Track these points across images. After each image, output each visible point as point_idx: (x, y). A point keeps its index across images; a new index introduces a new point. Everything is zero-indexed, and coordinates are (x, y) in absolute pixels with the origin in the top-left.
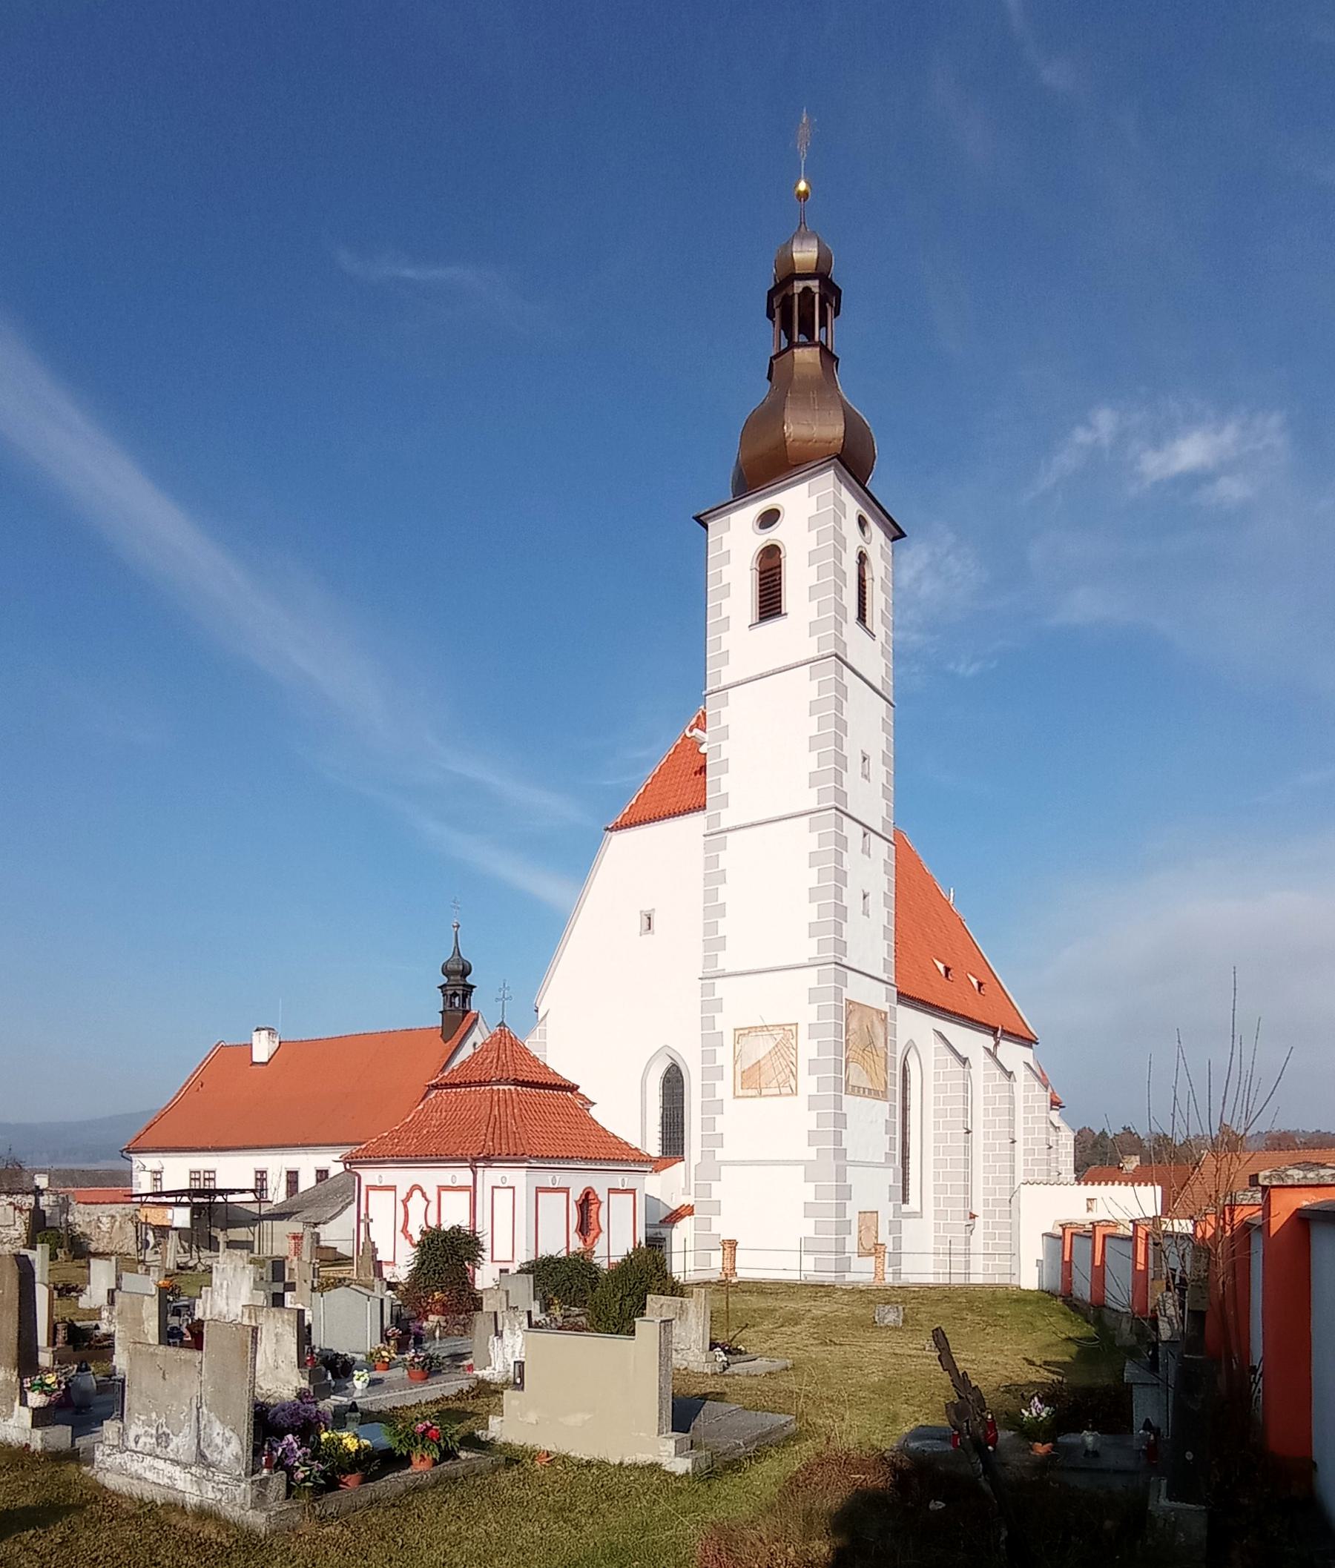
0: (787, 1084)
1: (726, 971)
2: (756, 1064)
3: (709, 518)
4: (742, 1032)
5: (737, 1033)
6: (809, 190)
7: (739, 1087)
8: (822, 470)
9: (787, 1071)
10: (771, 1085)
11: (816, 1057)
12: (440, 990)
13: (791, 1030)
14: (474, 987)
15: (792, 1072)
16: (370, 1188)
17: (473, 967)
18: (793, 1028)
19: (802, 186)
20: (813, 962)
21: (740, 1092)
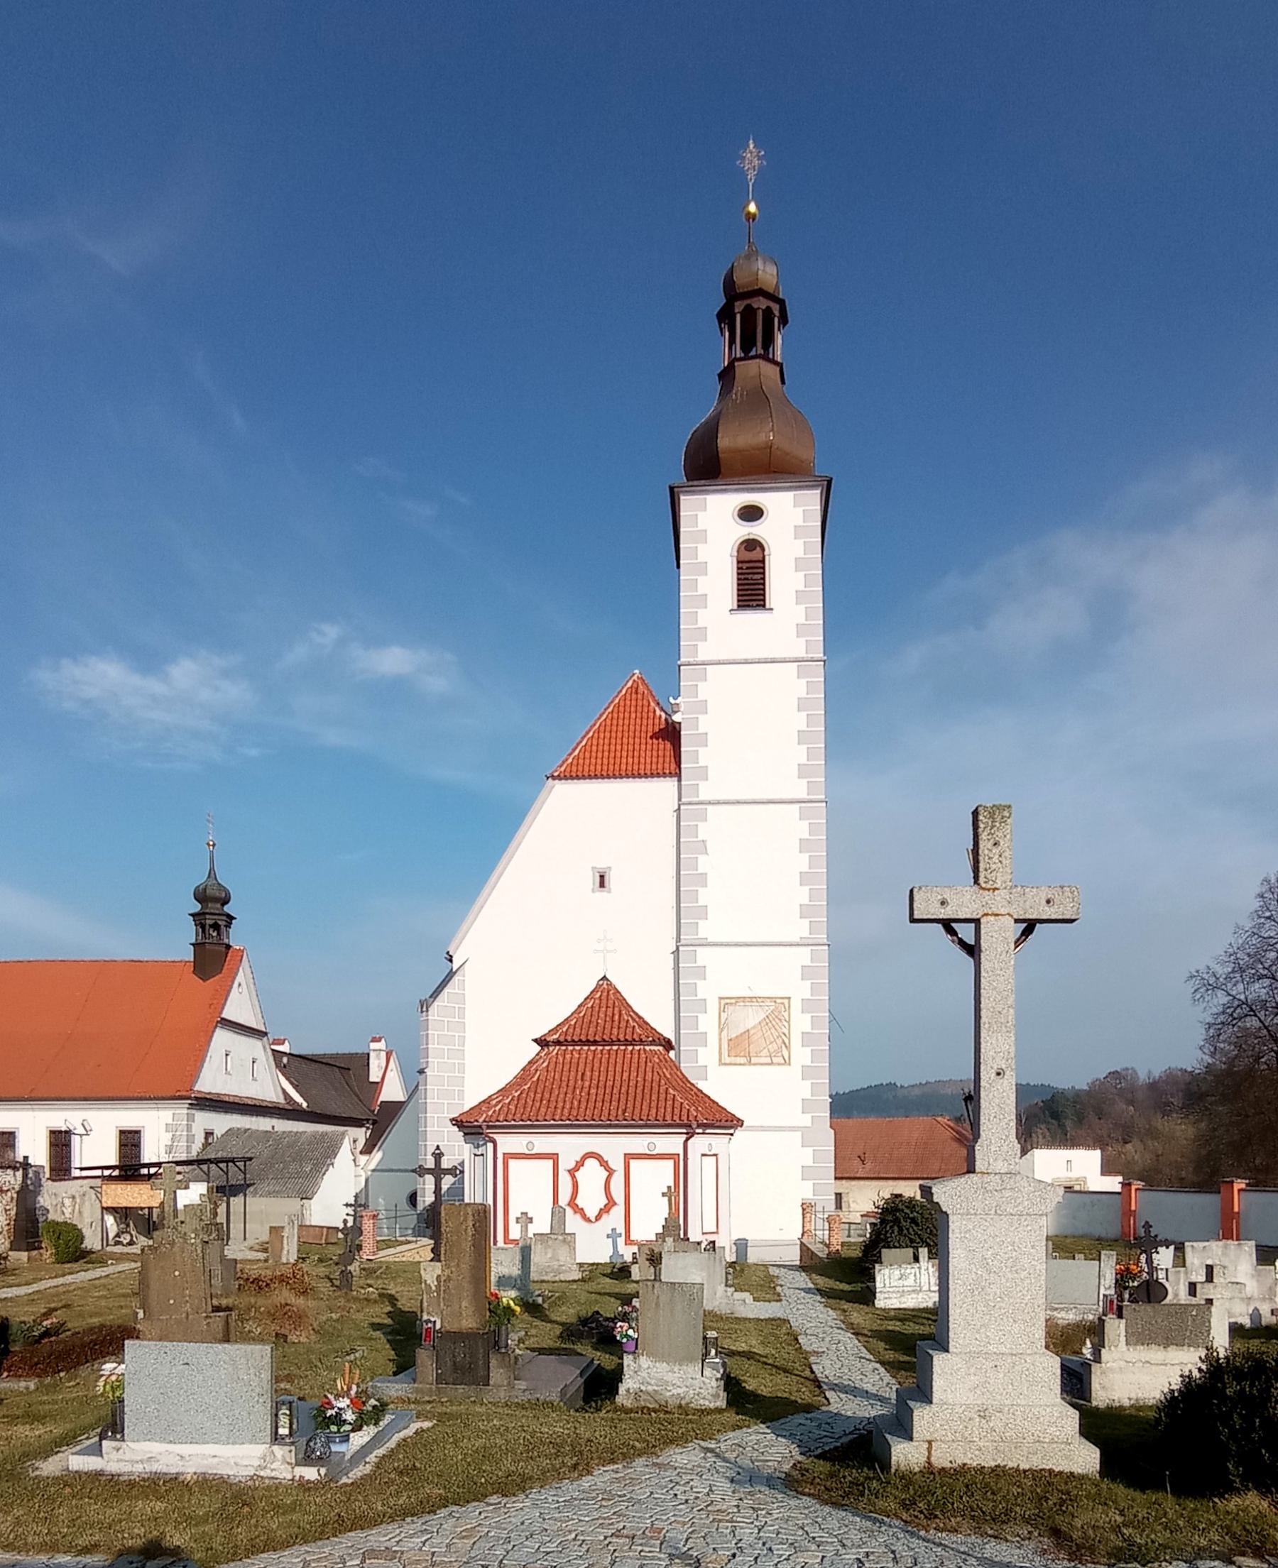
0: (780, 1054)
1: (709, 940)
2: (745, 1032)
3: (682, 492)
4: (728, 1001)
5: (723, 1002)
6: (758, 216)
7: (725, 1053)
8: (807, 486)
9: (779, 1041)
10: (762, 1054)
11: (810, 1031)
12: (191, 918)
13: (783, 1003)
14: (235, 918)
15: (785, 1043)
16: (508, 1156)
17: (231, 892)
18: (786, 1001)
19: (752, 208)
20: (806, 941)
21: (728, 1060)
